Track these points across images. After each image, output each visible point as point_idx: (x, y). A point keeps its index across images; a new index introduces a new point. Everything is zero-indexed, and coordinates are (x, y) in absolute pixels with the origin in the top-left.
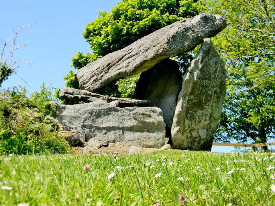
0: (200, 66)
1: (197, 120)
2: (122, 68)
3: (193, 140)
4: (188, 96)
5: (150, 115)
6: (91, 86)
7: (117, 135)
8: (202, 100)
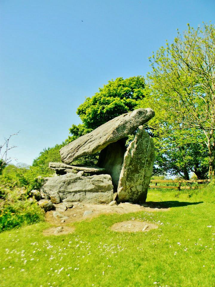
0: (135, 146)
2: (86, 149)
3: (133, 193)
5: (103, 181)
6: (67, 161)
7: (81, 196)
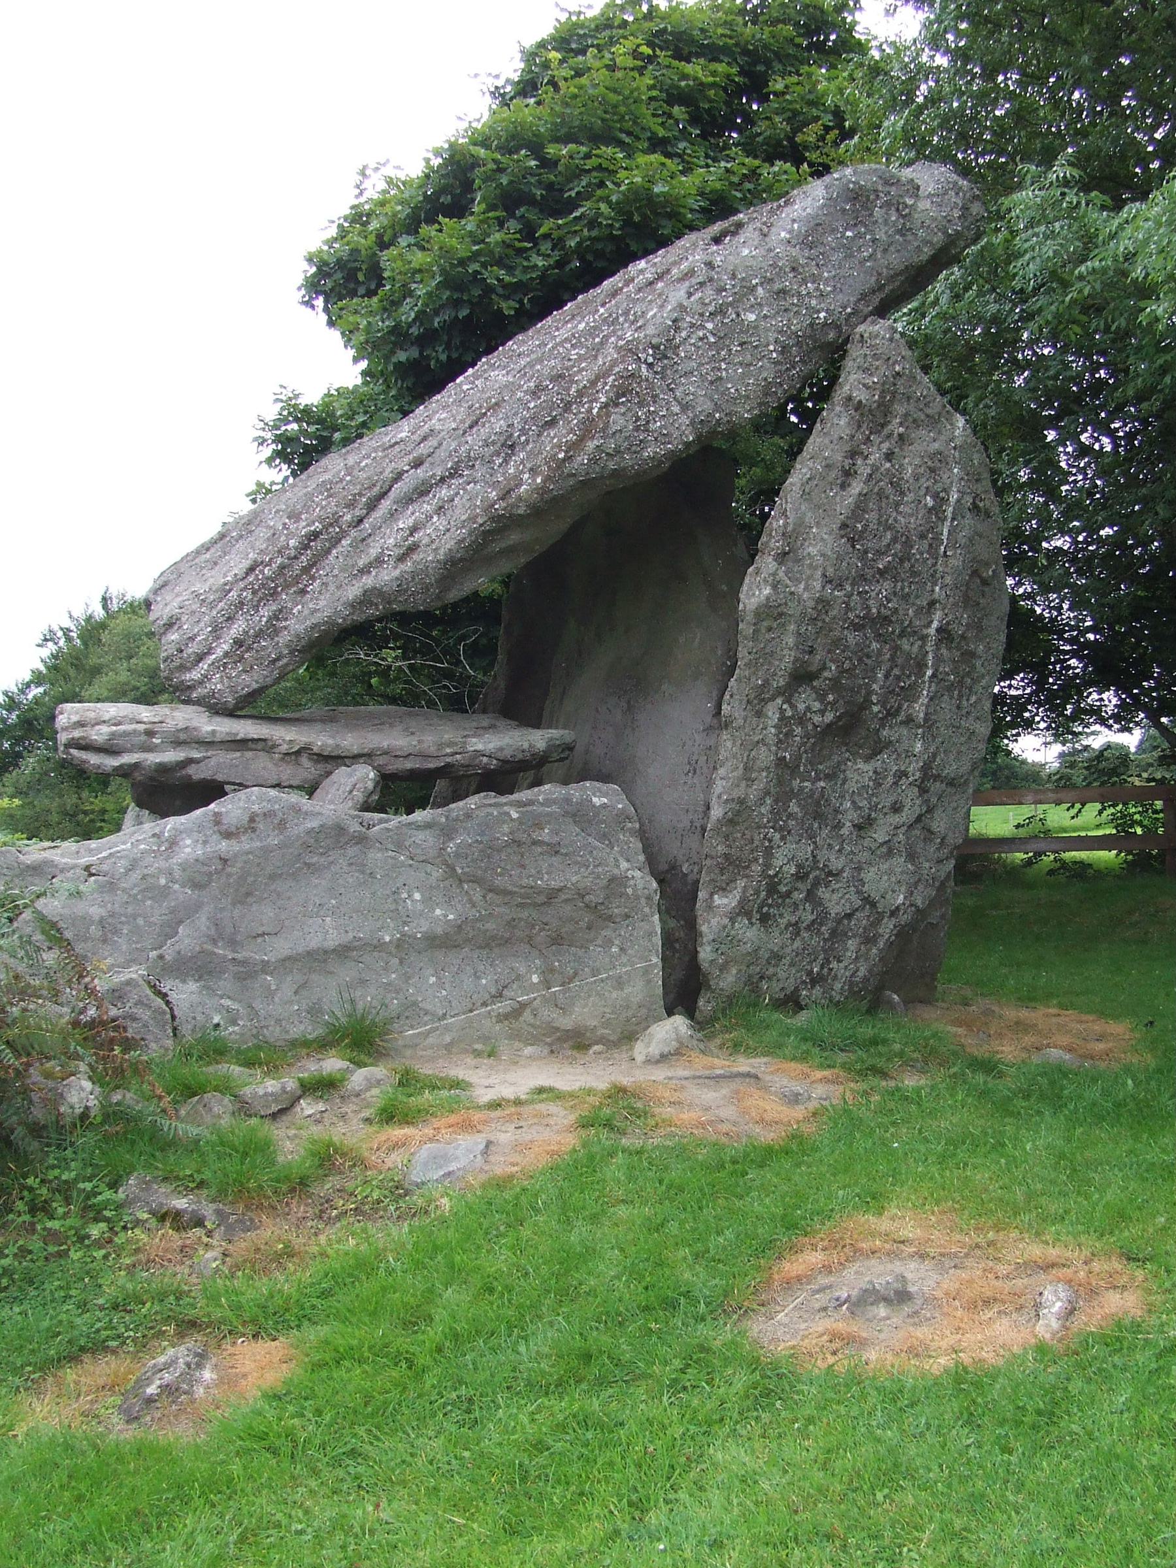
1: (850, 817)
4: (779, 701)
6: (216, 684)
8: (867, 702)
